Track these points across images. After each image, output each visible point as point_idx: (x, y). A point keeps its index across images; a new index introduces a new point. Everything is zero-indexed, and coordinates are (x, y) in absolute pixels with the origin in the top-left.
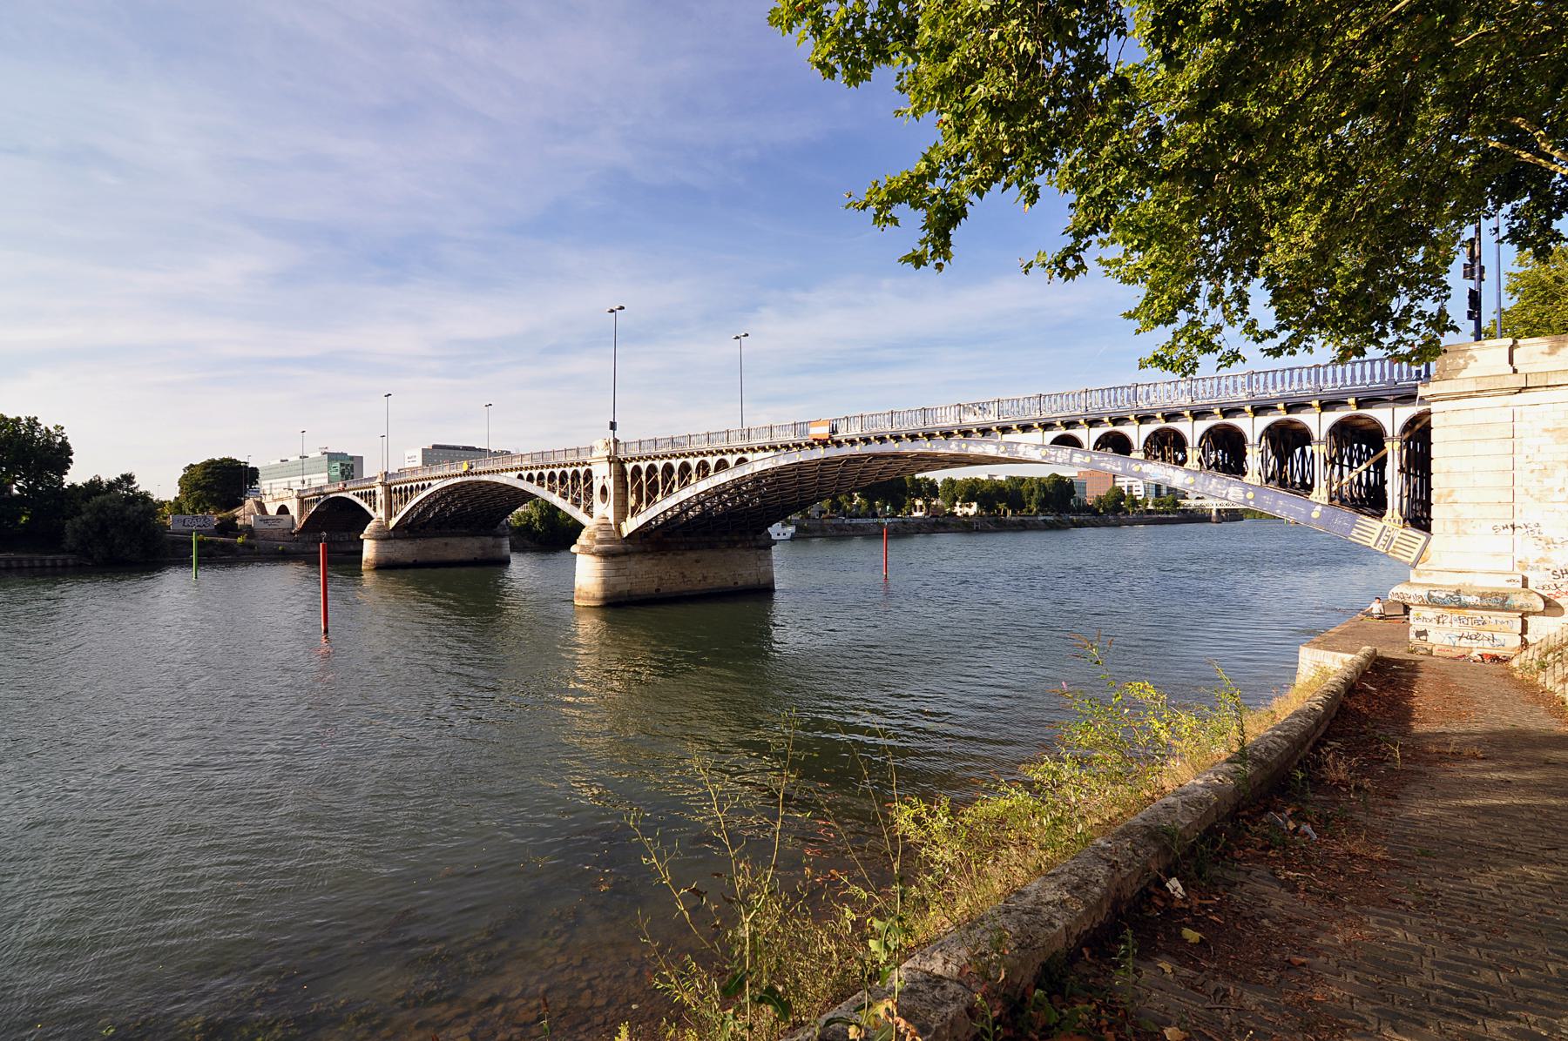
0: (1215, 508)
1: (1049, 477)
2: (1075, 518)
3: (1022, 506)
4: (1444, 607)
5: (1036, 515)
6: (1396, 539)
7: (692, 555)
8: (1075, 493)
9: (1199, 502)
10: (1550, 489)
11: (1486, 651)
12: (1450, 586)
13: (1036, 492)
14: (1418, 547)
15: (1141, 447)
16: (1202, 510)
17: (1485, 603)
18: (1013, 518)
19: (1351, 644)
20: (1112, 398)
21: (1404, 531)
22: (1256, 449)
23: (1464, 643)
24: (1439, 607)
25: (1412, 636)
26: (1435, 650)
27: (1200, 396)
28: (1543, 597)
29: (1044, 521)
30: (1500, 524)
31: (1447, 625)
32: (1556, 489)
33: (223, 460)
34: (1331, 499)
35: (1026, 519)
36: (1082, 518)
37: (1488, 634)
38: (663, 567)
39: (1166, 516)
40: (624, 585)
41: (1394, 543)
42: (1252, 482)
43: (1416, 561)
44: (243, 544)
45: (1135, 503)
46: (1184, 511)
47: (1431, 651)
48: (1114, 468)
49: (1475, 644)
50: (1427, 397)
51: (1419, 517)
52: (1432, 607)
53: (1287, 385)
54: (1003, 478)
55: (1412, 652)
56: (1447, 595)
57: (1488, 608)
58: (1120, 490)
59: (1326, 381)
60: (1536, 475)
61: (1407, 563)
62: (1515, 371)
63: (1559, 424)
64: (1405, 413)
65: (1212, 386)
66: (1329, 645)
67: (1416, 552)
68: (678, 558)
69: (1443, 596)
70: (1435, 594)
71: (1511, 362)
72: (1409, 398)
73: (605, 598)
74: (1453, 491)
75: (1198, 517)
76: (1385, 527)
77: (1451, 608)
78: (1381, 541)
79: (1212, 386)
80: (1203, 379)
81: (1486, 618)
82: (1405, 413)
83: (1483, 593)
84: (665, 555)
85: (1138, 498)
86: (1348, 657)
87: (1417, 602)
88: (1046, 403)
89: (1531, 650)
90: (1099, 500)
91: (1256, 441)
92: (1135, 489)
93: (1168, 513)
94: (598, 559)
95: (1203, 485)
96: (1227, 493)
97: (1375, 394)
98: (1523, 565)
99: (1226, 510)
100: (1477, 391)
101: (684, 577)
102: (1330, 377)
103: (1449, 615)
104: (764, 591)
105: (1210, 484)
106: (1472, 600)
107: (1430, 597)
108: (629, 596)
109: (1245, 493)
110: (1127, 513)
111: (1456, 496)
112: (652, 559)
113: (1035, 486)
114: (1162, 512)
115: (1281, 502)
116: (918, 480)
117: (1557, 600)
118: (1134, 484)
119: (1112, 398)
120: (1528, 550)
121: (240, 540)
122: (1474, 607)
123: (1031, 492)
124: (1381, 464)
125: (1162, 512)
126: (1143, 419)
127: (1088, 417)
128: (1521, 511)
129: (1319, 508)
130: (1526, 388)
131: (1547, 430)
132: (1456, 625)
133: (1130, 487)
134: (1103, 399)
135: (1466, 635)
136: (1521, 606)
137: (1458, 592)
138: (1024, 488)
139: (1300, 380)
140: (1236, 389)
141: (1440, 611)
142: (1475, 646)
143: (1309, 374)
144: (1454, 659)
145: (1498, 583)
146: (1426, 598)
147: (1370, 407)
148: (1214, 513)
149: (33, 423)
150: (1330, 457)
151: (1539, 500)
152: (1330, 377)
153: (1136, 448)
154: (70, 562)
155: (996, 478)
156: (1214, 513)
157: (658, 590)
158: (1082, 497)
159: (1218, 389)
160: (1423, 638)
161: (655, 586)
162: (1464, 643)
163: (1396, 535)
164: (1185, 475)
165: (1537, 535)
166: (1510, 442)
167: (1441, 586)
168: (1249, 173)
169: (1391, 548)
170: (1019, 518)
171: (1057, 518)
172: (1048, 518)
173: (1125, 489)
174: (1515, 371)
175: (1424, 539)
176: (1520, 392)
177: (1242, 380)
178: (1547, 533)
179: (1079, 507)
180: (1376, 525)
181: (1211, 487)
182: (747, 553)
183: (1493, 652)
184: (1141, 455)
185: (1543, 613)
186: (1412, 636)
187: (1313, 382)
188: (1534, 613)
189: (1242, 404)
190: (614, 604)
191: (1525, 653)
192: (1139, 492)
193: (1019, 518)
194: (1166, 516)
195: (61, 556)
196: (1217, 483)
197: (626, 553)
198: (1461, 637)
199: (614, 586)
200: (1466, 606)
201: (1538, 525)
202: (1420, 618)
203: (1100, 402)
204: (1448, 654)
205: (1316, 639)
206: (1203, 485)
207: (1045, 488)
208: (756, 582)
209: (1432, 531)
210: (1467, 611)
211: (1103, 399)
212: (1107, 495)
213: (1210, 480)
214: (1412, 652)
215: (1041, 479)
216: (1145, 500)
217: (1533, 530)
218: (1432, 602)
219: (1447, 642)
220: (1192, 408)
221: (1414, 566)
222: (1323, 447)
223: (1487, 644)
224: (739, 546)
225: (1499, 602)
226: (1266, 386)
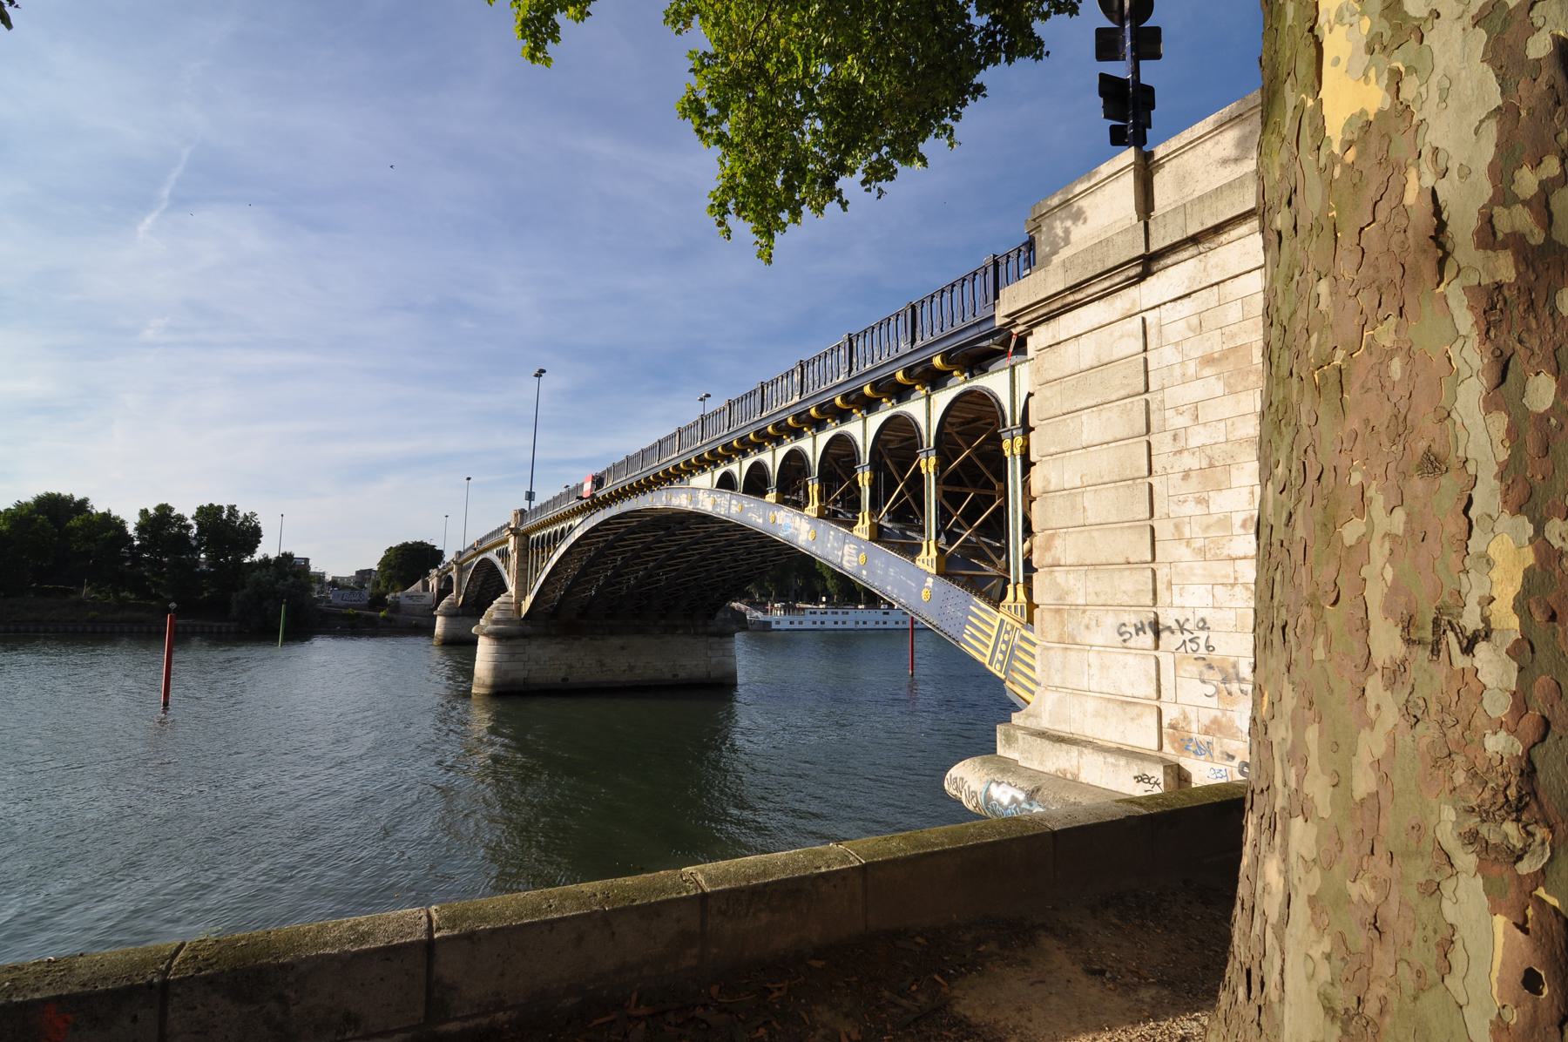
7: (615, 641)
30: (1131, 619)
33: (415, 543)
40: (519, 672)
44: (384, 617)
63: (1233, 336)
73: (494, 686)
76: (1002, 621)
94: (492, 642)
104: (722, 687)
121: (382, 614)
128: (1170, 584)
131: (1208, 360)
149: (60, 495)
151: (1202, 552)
154: (232, 629)
157: (565, 680)
161: (561, 674)
165: (1202, 651)
180: (995, 617)
190: (504, 691)
195: (227, 624)
197: (524, 636)
224: (680, 631)
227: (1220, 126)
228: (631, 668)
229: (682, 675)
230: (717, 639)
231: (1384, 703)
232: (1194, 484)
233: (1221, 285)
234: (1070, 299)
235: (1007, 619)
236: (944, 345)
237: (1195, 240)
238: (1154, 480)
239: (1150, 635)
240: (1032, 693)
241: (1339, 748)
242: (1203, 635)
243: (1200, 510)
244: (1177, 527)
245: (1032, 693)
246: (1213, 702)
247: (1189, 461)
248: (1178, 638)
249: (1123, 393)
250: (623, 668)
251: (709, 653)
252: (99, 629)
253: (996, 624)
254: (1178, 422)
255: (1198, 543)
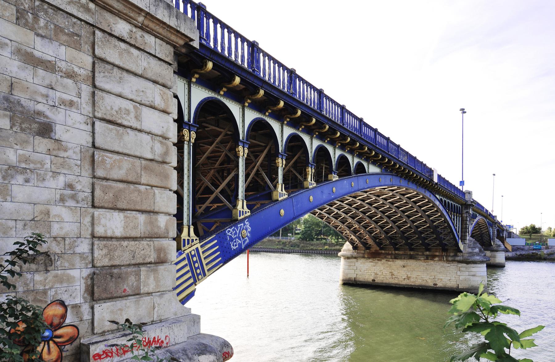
7: (399, 262)
28: (173, 93)
38: (378, 268)
68: (389, 263)
84: (381, 260)
88: (460, 277)
101: (392, 275)
108: (355, 280)
112: (372, 262)
113: (340, 170)
116: (215, 240)
157: (374, 280)
182: (448, 265)
199: (347, 274)
208: (455, 286)
224: (437, 259)
228: (408, 278)
229: (440, 284)
230: (464, 265)
233: (91, 134)
240: (178, 294)
245: (178, 294)
250: (404, 277)
251: (459, 273)
252: (328, 253)
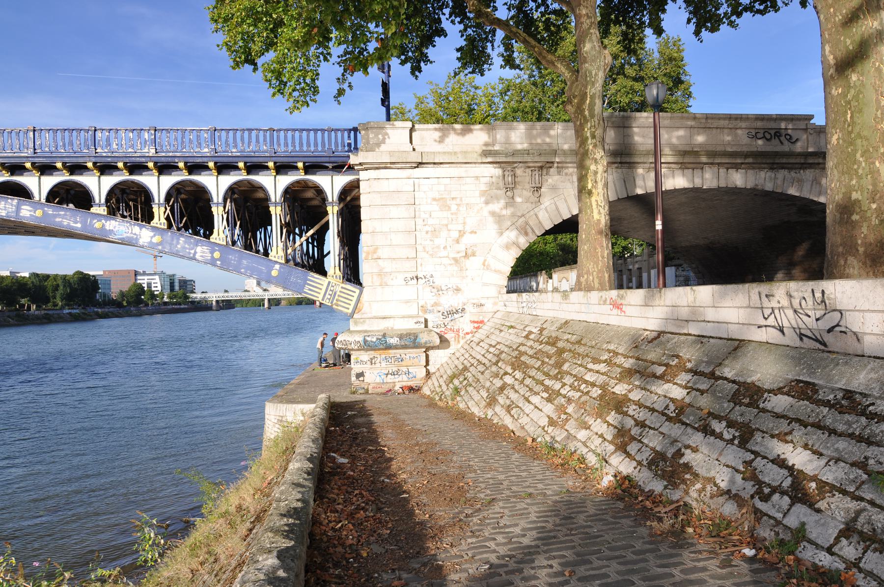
0: (214, 299)
1: (74, 274)
2: (100, 310)
3: (46, 300)
4: (375, 350)
5: (62, 308)
6: (338, 293)
8: (99, 288)
9: (203, 295)
10: (438, 247)
11: (404, 384)
12: (378, 331)
13: (61, 287)
14: (354, 299)
15: (103, 201)
16: (206, 301)
17: (403, 343)
18: (37, 313)
19: (308, 393)
20: (67, 141)
21: (344, 286)
22: (221, 208)
23: (390, 379)
24: (372, 350)
25: (353, 378)
26: (370, 388)
27: (164, 148)
29: (70, 314)
30: (409, 276)
31: (378, 365)
32: (442, 247)
34: (287, 261)
35: (50, 312)
36: (107, 310)
37: (405, 369)
39: (178, 307)
41: (336, 297)
42: (218, 242)
43: (354, 312)
45: (153, 296)
46: (193, 302)
47: (368, 390)
48: (72, 224)
49: (397, 379)
50: (357, 165)
51: (352, 274)
52: (367, 350)
53: (246, 145)
54: (27, 275)
55: (354, 393)
56: (377, 339)
57: (405, 347)
58: (140, 287)
59: (279, 145)
60: (429, 234)
61: (346, 314)
62: (414, 150)
63: (442, 195)
64: (341, 180)
65: (176, 139)
66: (290, 399)
67: (353, 303)
69: (374, 340)
70: (368, 339)
71: (411, 142)
72: (340, 167)
74: (377, 249)
75: (202, 307)
76: (329, 282)
77: (380, 349)
78: (328, 296)
79: (176, 139)
80: (167, 130)
81: (403, 356)
82: (341, 180)
83: (401, 335)
85: (156, 293)
86: (309, 408)
87: (356, 347)
89: (434, 378)
90: (122, 294)
91: (221, 200)
92: (153, 285)
93: (180, 304)
95: (171, 244)
96: (195, 253)
97: (319, 160)
98: (424, 309)
99: (223, 301)
100: (391, 163)
102: (282, 141)
103: (378, 356)
105: (178, 243)
106: (394, 341)
107: (365, 341)
109: (212, 252)
110: (147, 305)
111: (380, 253)
113: (60, 282)
114: (175, 304)
115: (245, 262)
117: (446, 336)
118: (153, 281)
119: (67, 141)
120: (427, 297)
122: (396, 347)
123: (56, 288)
124: (319, 239)
125: (175, 304)
126: (105, 168)
127: (36, 160)
128: (421, 265)
129: (277, 266)
130: (420, 163)
131: (434, 199)
132: (384, 364)
133: (149, 285)
134: (55, 141)
135: (391, 372)
136: (426, 343)
137: (384, 335)
138: (48, 284)
139: (258, 141)
140: (200, 144)
141: (372, 354)
142: (397, 380)
143: (265, 136)
144: (384, 394)
145: (408, 325)
146: (362, 343)
147: (314, 174)
148: (214, 303)
150: (285, 221)
151: (432, 255)
152: (282, 141)
153: (97, 201)
155: (19, 275)
156: (214, 303)
158: (107, 291)
159: (183, 142)
160: (361, 379)
162: (390, 379)
163: (338, 289)
164: (152, 234)
165: (431, 284)
166: (412, 207)
167: (373, 331)
168: (230, 41)
169: (335, 301)
170: (43, 312)
171: (83, 311)
172: (75, 311)
173: (145, 285)
174: (414, 150)
175: (358, 291)
176: (417, 167)
177: (205, 135)
178: (439, 281)
179: (104, 301)
181: (179, 246)
183: (409, 384)
184: (103, 210)
185: (438, 348)
186: (353, 378)
187: (268, 145)
188: (433, 348)
189: (205, 160)
191: (430, 382)
192: (157, 287)
193: (43, 312)
194: (178, 307)
196: (185, 242)
198: (387, 374)
200: (389, 347)
201: (432, 276)
202: (360, 361)
203: (52, 144)
204: (380, 390)
205: (280, 392)
206: (171, 244)
207: (70, 283)
209: (364, 285)
210: (390, 351)
211: (55, 141)
212: (129, 290)
213: (178, 239)
214: (354, 393)
215: (66, 276)
216: (162, 295)
217: (429, 279)
218: (367, 346)
219: (378, 380)
220: (156, 160)
221: (352, 316)
222: (279, 208)
223: (405, 378)
225: (410, 341)
226: (227, 144)
227: (436, 129)
231: (600, 263)
232: (429, 234)
234: (389, 166)
235: (332, 281)
236: (306, 159)
237: (434, 163)
238: (417, 233)
239: (416, 280)
241: (597, 266)
242: (431, 279)
243: (432, 243)
244: (424, 248)
246: (435, 297)
247: (428, 228)
248: (424, 280)
249: (406, 203)
253: (326, 284)
254: (423, 216)
255: (430, 253)
